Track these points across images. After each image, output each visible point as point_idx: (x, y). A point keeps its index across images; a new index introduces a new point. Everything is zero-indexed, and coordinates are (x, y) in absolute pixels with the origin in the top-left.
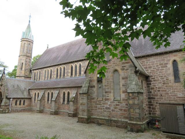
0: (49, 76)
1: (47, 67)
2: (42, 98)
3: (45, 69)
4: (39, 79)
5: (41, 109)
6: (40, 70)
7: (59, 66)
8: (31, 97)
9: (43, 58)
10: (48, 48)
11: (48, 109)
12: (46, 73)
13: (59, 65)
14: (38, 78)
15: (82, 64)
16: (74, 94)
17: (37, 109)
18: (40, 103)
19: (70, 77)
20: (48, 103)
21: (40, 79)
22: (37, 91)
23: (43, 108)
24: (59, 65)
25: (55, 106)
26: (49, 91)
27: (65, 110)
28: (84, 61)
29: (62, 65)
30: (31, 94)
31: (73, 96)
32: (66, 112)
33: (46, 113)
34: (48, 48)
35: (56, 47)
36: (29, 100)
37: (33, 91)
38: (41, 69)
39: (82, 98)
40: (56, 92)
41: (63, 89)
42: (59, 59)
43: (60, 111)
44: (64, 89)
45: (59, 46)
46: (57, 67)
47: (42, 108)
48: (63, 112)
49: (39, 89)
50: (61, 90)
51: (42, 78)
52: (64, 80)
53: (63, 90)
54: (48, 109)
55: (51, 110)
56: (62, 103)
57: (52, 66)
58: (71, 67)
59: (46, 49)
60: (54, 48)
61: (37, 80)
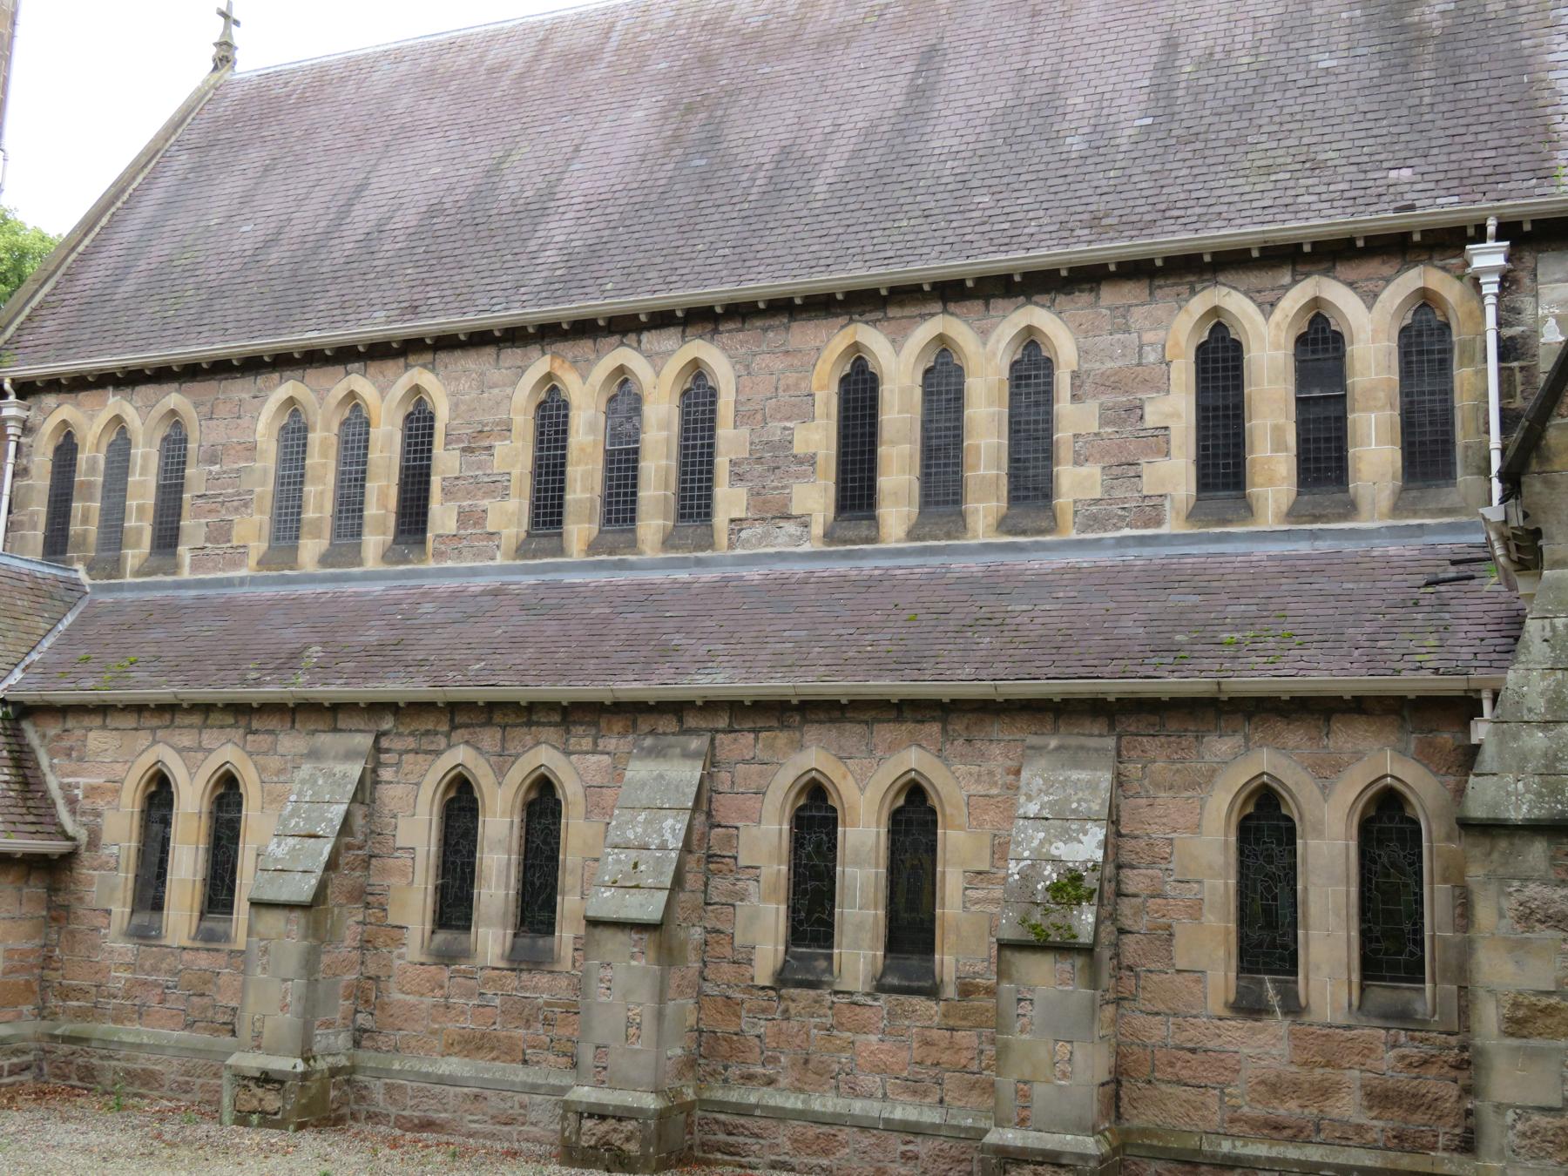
0: (371, 510)
1: (345, 355)
2: (332, 865)
3: (286, 388)
4: (167, 538)
5: (322, 1065)
6: (173, 398)
7: (584, 347)
8: (55, 846)
9: (168, 204)
10: (224, 56)
11: (452, 1066)
12: (313, 459)
13: (584, 329)
14: (140, 523)
15: (1078, 329)
16: (1063, 820)
17: (252, 1062)
18: (310, 963)
19: (829, 537)
20: (446, 957)
21: (184, 552)
22: (186, 739)
23: (342, 1041)
24: (584, 329)
25: (660, 1016)
26: (460, 755)
27: (854, 1092)
28: (1110, 295)
29: (663, 340)
30: (53, 783)
31: (1060, 849)
32: (864, 1126)
33: (427, 1125)
34: (224, 56)
35: (396, 56)
36: (35, 889)
37: (99, 740)
38: (198, 387)
39: (1527, 917)
40: (640, 770)
41: (782, 738)
42: (559, 231)
43: (744, 1111)
44: (812, 733)
45: (456, 46)
46: (540, 364)
47: (334, 1045)
48: (817, 1119)
49: (240, 711)
50: (739, 745)
51: (221, 532)
52: (273, 604)
53: (801, 747)
54: (452, 1066)
55: (585, 1094)
56: (763, 974)
57: (446, 343)
58: (58, 450)
59: (195, 72)
60: (355, 69)
61: (108, 563)
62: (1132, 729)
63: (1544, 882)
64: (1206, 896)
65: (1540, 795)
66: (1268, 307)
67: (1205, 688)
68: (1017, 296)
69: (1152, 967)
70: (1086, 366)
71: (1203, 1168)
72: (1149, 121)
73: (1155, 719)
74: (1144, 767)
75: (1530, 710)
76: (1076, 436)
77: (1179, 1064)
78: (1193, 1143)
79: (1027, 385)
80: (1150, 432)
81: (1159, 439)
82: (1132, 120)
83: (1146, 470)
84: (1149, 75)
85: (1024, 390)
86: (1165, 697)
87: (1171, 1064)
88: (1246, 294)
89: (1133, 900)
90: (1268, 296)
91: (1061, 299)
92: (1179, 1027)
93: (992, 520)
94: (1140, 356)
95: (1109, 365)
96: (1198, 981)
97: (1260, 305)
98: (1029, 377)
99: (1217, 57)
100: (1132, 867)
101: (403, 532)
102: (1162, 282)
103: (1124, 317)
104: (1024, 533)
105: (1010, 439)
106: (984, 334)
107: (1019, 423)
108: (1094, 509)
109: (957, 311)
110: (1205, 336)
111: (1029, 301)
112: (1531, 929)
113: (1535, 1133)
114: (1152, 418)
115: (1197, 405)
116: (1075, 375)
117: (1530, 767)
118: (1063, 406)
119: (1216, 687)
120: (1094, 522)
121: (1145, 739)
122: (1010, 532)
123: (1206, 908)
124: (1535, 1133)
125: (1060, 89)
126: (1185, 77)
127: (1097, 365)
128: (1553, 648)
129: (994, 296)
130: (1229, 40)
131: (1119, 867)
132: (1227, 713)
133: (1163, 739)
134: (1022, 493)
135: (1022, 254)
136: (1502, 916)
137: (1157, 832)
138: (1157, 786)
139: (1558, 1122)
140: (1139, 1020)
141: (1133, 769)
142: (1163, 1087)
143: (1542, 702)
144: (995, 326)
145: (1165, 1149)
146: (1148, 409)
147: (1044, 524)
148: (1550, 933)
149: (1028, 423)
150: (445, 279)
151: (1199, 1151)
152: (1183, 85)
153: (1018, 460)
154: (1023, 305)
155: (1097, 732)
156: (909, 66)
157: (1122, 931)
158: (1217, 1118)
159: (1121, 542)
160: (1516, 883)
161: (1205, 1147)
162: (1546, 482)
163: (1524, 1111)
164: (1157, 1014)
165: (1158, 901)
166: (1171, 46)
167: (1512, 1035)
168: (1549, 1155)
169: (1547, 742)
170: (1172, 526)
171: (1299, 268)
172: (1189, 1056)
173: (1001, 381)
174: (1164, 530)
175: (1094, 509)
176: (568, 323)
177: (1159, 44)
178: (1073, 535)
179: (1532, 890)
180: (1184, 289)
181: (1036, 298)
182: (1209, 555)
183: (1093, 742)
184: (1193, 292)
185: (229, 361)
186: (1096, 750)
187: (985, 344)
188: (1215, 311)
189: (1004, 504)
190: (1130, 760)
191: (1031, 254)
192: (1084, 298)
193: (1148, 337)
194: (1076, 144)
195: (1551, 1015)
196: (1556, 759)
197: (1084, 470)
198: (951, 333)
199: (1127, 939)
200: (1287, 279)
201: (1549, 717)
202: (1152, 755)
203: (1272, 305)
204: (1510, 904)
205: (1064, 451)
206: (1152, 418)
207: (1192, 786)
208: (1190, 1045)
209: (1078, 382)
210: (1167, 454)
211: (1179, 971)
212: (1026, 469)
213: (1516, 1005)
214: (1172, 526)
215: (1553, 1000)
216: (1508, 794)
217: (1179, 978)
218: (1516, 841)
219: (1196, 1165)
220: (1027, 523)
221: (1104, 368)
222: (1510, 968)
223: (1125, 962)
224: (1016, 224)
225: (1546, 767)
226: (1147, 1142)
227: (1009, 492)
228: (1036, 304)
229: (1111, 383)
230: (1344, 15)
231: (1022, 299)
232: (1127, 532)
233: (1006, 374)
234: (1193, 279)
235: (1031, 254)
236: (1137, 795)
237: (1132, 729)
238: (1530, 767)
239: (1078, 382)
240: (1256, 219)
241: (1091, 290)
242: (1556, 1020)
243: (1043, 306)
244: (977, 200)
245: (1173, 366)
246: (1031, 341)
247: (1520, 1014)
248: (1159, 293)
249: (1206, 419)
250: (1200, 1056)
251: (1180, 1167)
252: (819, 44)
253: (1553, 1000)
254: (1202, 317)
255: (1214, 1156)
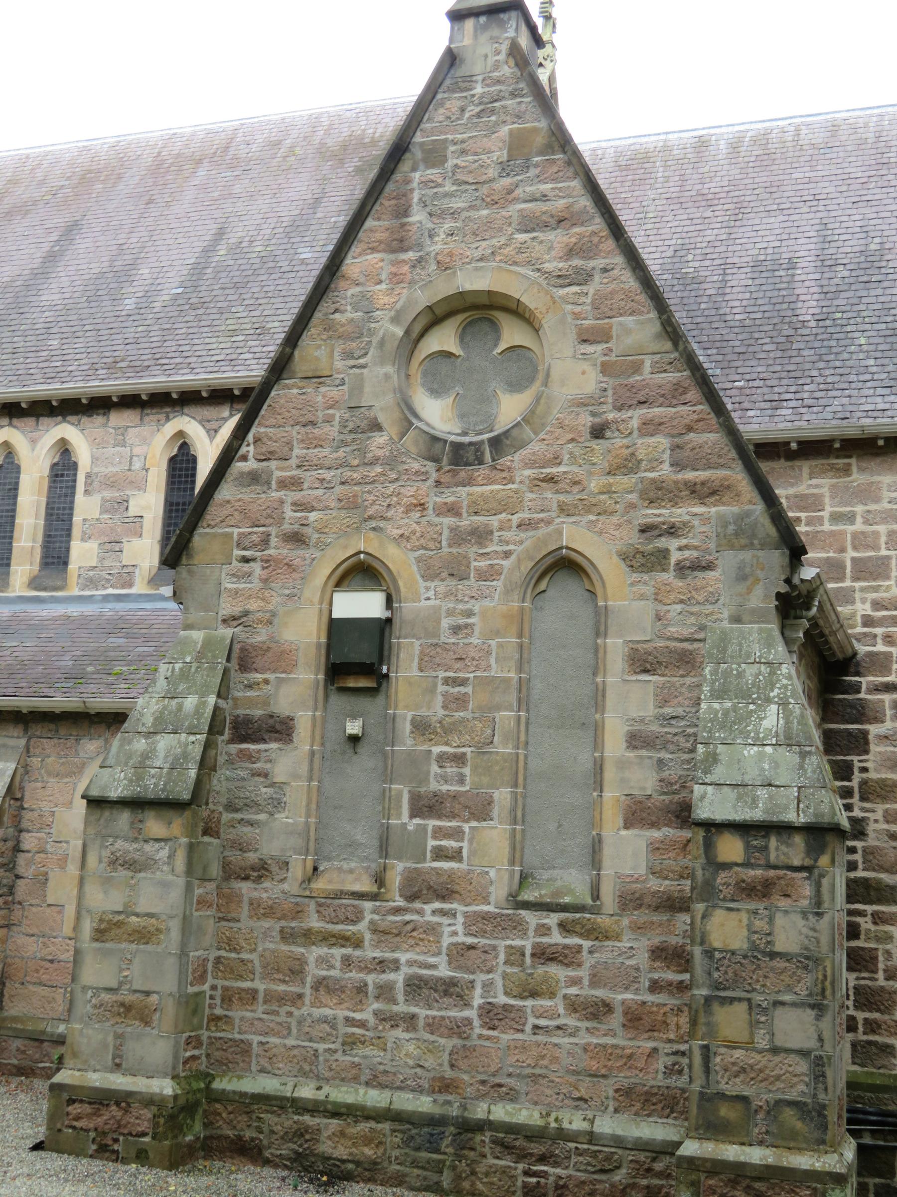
15: (94, 443)
28: (118, 419)
39: (113, 862)
62: (38, 733)
63: (126, 839)
64: (70, 852)
65: (131, 781)
66: (213, 433)
67: (76, 705)
68: (57, 416)
69: (33, 902)
70: (96, 470)
71: (46, 1044)
72: (180, 290)
73: (52, 726)
74: (43, 760)
75: (143, 725)
76: (85, 520)
77: (42, 971)
78: (41, 1026)
79: (61, 482)
80: (131, 520)
81: (135, 525)
82: (172, 288)
83: (126, 546)
84: (197, 255)
85: (59, 485)
86: (57, 711)
87: (37, 971)
88: (200, 422)
89: (27, 855)
90: (214, 425)
91: (85, 419)
92: (44, 944)
93: (25, 579)
94: (131, 464)
95: (111, 469)
96: (60, 912)
97: (208, 431)
98: (62, 475)
99: (243, 245)
100: (28, 831)
101: (47, 564)
102: (149, 411)
103: (123, 435)
104: (45, 589)
105: (46, 520)
106: (34, 442)
107: (53, 508)
108: (91, 573)
109: (18, 425)
110: (175, 451)
111: (64, 420)
112: (115, 870)
113: (101, 1005)
114: (133, 511)
115: (167, 501)
116: (88, 476)
117: (131, 762)
118: (80, 498)
119: (82, 705)
120: (91, 583)
121: (45, 740)
122: (36, 589)
123: (69, 861)
124: (101, 1005)
125: (139, 261)
126: (217, 258)
127: (103, 469)
128: (169, 683)
129: (42, 415)
130: (256, 233)
131: (21, 831)
132: (96, 723)
133: (56, 741)
134: (50, 560)
135: (58, 386)
136: (100, 861)
137: (46, 807)
138: (49, 774)
139: (114, 998)
140: (21, 940)
141: (35, 761)
142: (31, 987)
143: (151, 720)
144: (41, 437)
145: (22, 1030)
146: (132, 503)
147: (59, 583)
148: (125, 872)
149: (59, 509)
150: (215, 346)
151: (43, 1032)
152: (213, 265)
153: (49, 536)
154: (60, 423)
155: (16, 734)
156: (54, 237)
157: (18, 877)
158: (61, 1009)
159: (106, 598)
160: (111, 840)
161: (49, 1029)
162: (190, 572)
163: (97, 990)
164: (33, 935)
165: (42, 855)
166: (220, 234)
167: (97, 940)
168: (108, 1020)
169: (145, 746)
170: (140, 587)
171: (235, 406)
172: (48, 965)
173: (41, 477)
174: (133, 591)
175: (91, 573)
176: (118, 397)
177: (213, 232)
178: (76, 592)
179: (120, 844)
180: (162, 417)
181: (69, 418)
182: (153, 610)
183: (11, 742)
184: (168, 419)
185: (198, 392)
186: (12, 748)
187: (33, 450)
188: (181, 434)
189: (36, 568)
190: (35, 756)
191: (65, 386)
192: (99, 420)
193: (137, 450)
194: (129, 304)
195: (119, 927)
196: (148, 758)
197: (87, 545)
198: (12, 441)
199: (20, 882)
200: (226, 413)
201: (152, 730)
202: (48, 752)
203: (216, 431)
204: (106, 853)
205: (76, 532)
206: (133, 511)
207: (69, 774)
208: (50, 957)
209: (89, 481)
210: (141, 536)
211: (49, 905)
212: (55, 542)
213: (101, 920)
214: (140, 587)
215: (121, 917)
216: (114, 780)
217: (48, 910)
218: (115, 812)
219: (42, 1041)
220: (49, 582)
221: (107, 471)
222: (101, 896)
223: (17, 899)
224: (65, 363)
225: (140, 762)
226: (14, 1025)
227: (42, 558)
228: (69, 422)
229: (110, 483)
230: (333, 219)
231: (60, 418)
232: (111, 591)
233: (46, 472)
234: (168, 410)
235: (65, 386)
236: (36, 780)
237: (38, 733)
238: (131, 762)
239: (89, 481)
240: (209, 369)
241: (104, 414)
242: (122, 931)
243: (73, 424)
244: (50, 343)
245: (150, 472)
246: (64, 449)
247: (103, 926)
248: (147, 419)
249: (171, 511)
250: (55, 965)
251: (32, 1043)
252: (7, 213)
253: (121, 917)
254: (171, 438)
255: (52, 1035)
